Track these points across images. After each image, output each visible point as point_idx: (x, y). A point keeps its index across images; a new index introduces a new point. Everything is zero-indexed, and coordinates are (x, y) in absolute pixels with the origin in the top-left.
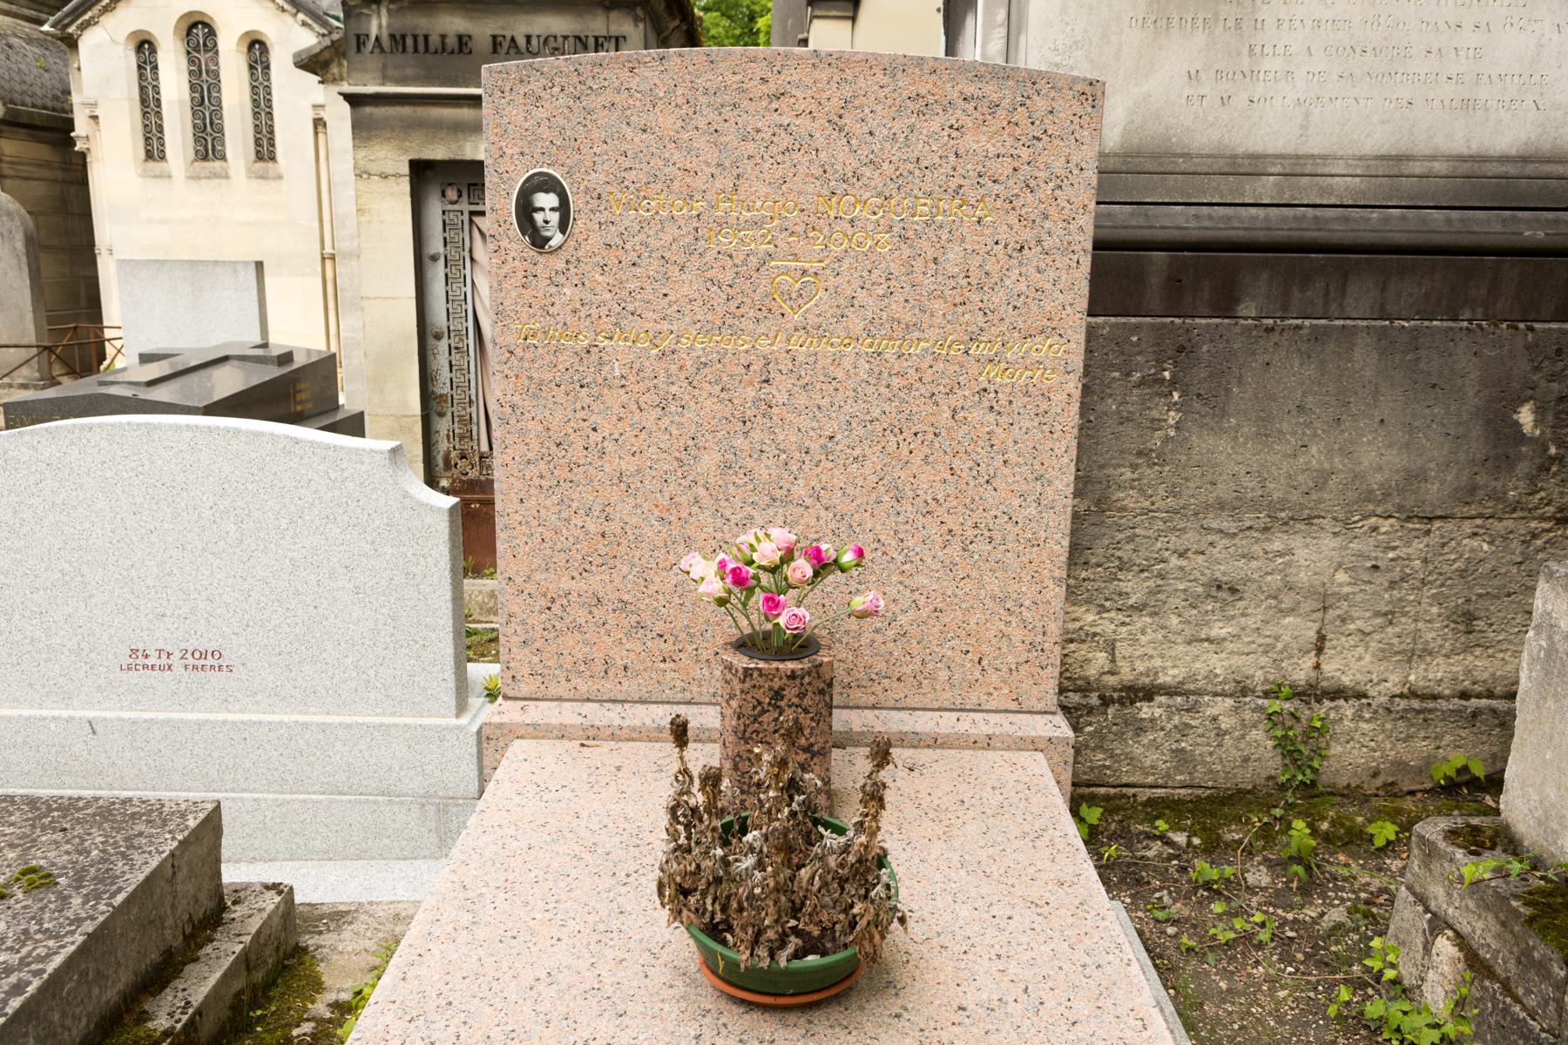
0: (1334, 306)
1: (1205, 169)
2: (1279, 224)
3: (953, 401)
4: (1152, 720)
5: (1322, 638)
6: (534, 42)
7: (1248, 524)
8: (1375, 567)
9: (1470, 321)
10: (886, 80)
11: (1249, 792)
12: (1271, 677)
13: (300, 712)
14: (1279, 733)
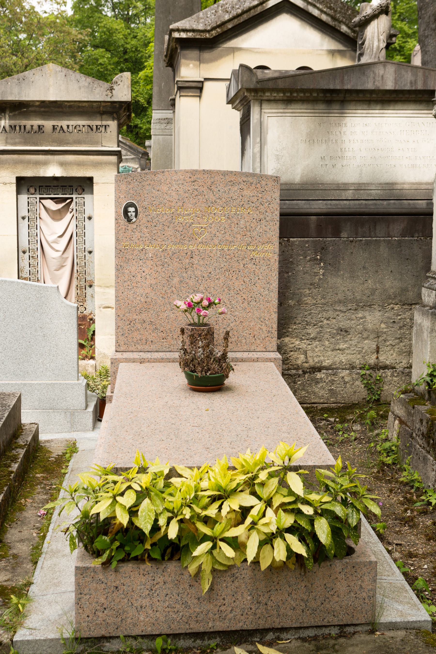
0: (372, 233)
1: (329, 188)
2: (354, 206)
3: (244, 262)
4: (321, 379)
5: (378, 348)
6: (70, 128)
7: (349, 308)
8: (394, 322)
9: (418, 237)
10: (223, 177)
11: (357, 404)
12: (362, 362)
13: (22, 380)
14: (365, 382)
